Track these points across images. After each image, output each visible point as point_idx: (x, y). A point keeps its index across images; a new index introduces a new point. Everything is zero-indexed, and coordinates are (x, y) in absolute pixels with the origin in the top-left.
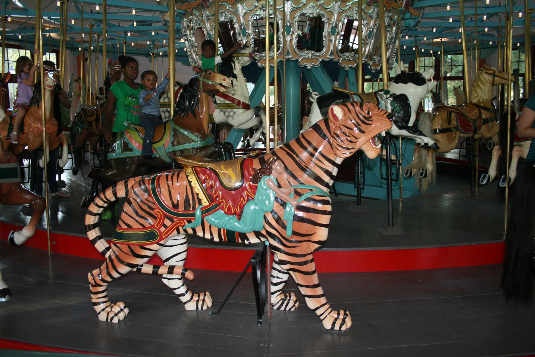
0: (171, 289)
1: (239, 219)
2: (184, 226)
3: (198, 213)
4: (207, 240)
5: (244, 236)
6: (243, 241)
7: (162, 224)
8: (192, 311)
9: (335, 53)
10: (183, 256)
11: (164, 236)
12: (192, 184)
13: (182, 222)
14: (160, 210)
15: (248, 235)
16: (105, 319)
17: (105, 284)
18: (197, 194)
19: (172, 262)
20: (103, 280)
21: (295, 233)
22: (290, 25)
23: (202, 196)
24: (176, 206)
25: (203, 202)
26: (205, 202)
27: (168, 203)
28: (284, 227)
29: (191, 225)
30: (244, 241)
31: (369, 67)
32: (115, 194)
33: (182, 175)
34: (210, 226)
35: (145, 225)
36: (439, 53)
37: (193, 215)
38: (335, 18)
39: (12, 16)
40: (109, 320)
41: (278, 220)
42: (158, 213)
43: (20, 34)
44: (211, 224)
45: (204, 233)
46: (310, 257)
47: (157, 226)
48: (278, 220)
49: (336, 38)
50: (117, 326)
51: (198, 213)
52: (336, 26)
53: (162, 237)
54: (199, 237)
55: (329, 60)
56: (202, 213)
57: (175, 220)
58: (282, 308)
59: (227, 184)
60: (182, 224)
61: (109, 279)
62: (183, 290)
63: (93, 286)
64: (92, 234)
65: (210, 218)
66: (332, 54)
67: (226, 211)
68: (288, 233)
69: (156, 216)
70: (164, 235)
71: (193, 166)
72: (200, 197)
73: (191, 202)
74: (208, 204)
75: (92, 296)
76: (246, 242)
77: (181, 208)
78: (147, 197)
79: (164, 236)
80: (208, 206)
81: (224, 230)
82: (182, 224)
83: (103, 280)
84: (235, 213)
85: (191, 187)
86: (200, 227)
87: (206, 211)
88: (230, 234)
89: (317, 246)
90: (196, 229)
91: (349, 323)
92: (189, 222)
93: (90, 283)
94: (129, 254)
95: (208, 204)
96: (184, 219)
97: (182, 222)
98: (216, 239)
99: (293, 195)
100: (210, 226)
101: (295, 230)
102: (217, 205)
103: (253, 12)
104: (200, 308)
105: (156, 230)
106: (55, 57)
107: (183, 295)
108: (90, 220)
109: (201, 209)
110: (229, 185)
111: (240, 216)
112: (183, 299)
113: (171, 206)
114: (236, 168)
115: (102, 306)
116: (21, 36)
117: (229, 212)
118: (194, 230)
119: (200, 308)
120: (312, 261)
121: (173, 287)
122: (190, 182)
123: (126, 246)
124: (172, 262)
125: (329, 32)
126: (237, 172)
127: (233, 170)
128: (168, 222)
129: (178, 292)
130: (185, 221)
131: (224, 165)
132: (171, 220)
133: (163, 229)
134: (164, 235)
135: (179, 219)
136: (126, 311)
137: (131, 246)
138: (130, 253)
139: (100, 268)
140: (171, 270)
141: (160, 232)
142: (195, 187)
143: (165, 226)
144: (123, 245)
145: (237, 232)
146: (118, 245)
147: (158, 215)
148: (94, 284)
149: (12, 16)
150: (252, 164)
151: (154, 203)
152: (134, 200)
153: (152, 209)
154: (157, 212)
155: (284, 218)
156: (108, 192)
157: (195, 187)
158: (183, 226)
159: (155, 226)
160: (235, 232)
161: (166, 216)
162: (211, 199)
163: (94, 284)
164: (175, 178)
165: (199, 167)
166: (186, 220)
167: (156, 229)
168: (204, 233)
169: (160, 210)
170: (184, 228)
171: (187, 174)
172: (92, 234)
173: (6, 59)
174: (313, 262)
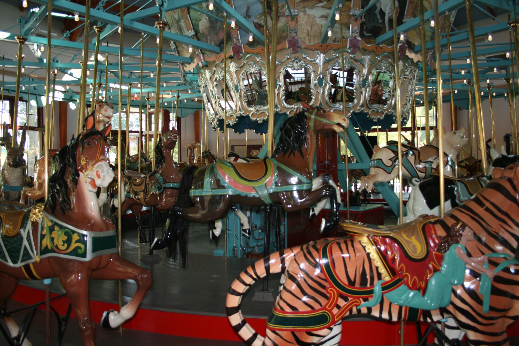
1: (424, 294)
3: (377, 288)
4: (385, 321)
5: (427, 313)
6: (425, 319)
9: (365, 105)
15: (433, 313)
18: (377, 268)
21: (492, 309)
22: (323, 77)
24: (352, 283)
26: (387, 278)
30: (427, 319)
31: (368, 116)
32: (267, 269)
34: (391, 304)
35: (314, 307)
36: (506, 95)
37: (372, 292)
38: (365, 71)
39: (25, 67)
42: (331, 292)
43: (24, 86)
45: (381, 313)
46: (505, 336)
47: (329, 307)
49: (366, 90)
51: (377, 288)
52: (367, 79)
55: (359, 111)
56: (384, 289)
64: (235, 319)
65: (392, 295)
66: (362, 106)
67: (411, 286)
68: (485, 308)
69: (328, 295)
70: (337, 318)
72: (380, 271)
73: (368, 277)
76: (429, 320)
78: (319, 274)
80: (389, 281)
81: (406, 308)
82: (358, 302)
84: (419, 289)
85: (370, 260)
86: (378, 306)
88: (413, 312)
89: (511, 321)
90: (373, 309)
94: (292, 342)
98: (395, 319)
99: (486, 266)
100: (391, 304)
101: (493, 305)
102: (399, 280)
103: (285, 64)
106: (430, 123)
108: (233, 301)
109: (382, 285)
113: (347, 283)
116: (25, 70)
117: (414, 287)
118: (369, 309)
123: (289, 333)
125: (360, 84)
130: (361, 299)
131: (404, 233)
132: (346, 299)
133: (335, 311)
134: (337, 318)
135: (355, 298)
137: (296, 333)
138: (293, 340)
141: (332, 314)
143: (338, 307)
144: (285, 332)
146: (277, 331)
147: (330, 294)
149: (25, 67)
151: (326, 280)
153: (323, 287)
154: (331, 290)
158: (357, 306)
162: (392, 271)
168: (381, 313)
170: (358, 308)
171: (364, 245)
172: (235, 319)
173: (435, 117)
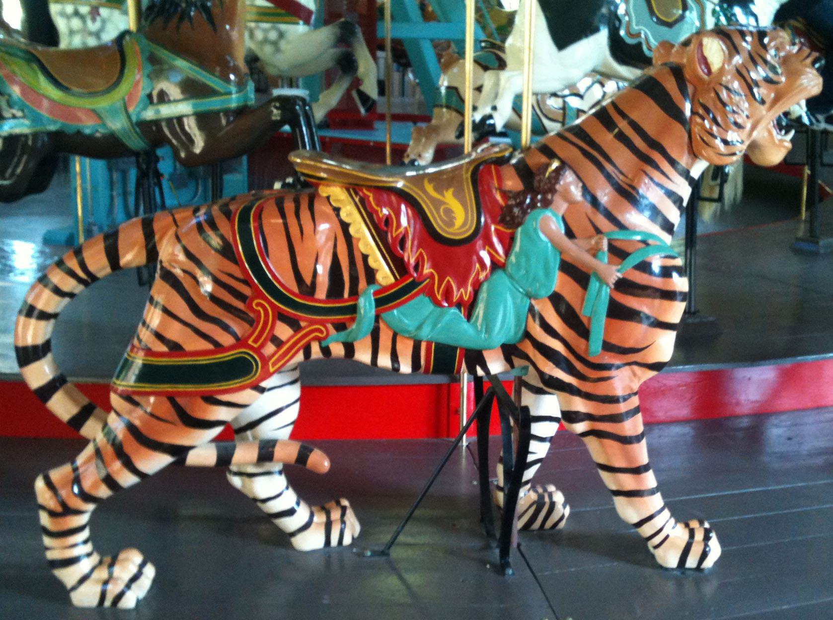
0: (255, 500)
2: (325, 338)
3: (366, 304)
5: (475, 358)
7: (270, 335)
8: (313, 552)
10: (293, 413)
11: (273, 366)
12: (352, 230)
13: (322, 328)
14: (266, 300)
15: (486, 354)
16: (93, 601)
17: (91, 507)
18: (365, 257)
19: (268, 430)
20: (86, 497)
21: (608, 347)
23: (378, 261)
25: (379, 277)
26: (385, 275)
27: (285, 278)
28: (584, 332)
29: (343, 335)
33: (321, 207)
37: (353, 309)
40: (108, 603)
41: (570, 317)
42: (260, 308)
44: (397, 331)
47: (255, 341)
48: (570, 317)
50: (134, 614)
53: (268, 369)
54: (360, 364)
57: (303, 324)
58: (537, 525)
59: (441, 227)
60: (321, 332)
61: (104, 492)
62: (289, 499)
63: (52, 514)
68: (595, 347)
70: (274, 364)
71: (350, 184)
72: (371, 263)
74: (392, 280)
75: (47, 541)
77: (321, 293)
79: (273, 366)
80: (391, 286)
81: (429, 344)
82: (321, 332)
83: (86, 497)
87: (385, 300)
90: (357, 345)
91: (715, 549)
92: (340, 327)
93: (43, 508)
95: (392, 280)
96: (328, 321)
97: (322, 328)
102: (414, 285)
104: (334, 541)
105: (251, 353)
107: (291, 512)
110: (449, 233)
111: (469, 308)
112: (290, 524)
114: (463, 190)
115: (85, 566)
119: (334, 541)
120: (636, 411)
121: (262, 495)
122: (345, 226)
124: (268, 430)
126: (465, 197)
127: (455, 195)
128: (283, 331)
129: (275, 506)
130: (330, 326)
132: (294, 323)
133: (270, 348)
134: (274, 364)
136: (150, 572)
137: (180, 401)
138: (172, 415)
139: (73, 461)
140: (266, 452)
142: (359, 239)
143: (278, 343)
145: (461, 349)
148: (59, 509)
150: (500, 179)
151: (247, 282)
152: (187, 276)
154: (258, 304)
155: (584, 313)
156: (163, 247)
157: (359, 239)
158: (319, 340)
159: (250, 342)
160: (454, 349)
161: (283, 317)
162: (398, 265)
163: (59, 509)
164: (305, 214)
165: (369, 188)
166: (333, 324)
167: (251, 348)
169: (266, 300)
170: (324, 344)
174: (639, 412)
